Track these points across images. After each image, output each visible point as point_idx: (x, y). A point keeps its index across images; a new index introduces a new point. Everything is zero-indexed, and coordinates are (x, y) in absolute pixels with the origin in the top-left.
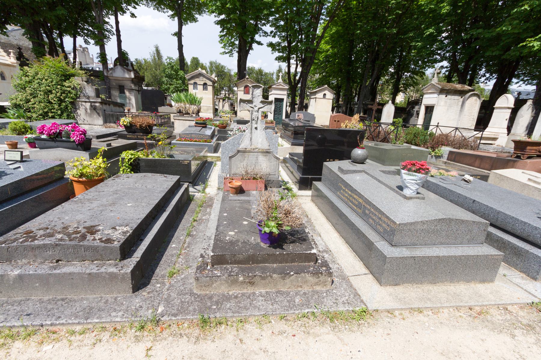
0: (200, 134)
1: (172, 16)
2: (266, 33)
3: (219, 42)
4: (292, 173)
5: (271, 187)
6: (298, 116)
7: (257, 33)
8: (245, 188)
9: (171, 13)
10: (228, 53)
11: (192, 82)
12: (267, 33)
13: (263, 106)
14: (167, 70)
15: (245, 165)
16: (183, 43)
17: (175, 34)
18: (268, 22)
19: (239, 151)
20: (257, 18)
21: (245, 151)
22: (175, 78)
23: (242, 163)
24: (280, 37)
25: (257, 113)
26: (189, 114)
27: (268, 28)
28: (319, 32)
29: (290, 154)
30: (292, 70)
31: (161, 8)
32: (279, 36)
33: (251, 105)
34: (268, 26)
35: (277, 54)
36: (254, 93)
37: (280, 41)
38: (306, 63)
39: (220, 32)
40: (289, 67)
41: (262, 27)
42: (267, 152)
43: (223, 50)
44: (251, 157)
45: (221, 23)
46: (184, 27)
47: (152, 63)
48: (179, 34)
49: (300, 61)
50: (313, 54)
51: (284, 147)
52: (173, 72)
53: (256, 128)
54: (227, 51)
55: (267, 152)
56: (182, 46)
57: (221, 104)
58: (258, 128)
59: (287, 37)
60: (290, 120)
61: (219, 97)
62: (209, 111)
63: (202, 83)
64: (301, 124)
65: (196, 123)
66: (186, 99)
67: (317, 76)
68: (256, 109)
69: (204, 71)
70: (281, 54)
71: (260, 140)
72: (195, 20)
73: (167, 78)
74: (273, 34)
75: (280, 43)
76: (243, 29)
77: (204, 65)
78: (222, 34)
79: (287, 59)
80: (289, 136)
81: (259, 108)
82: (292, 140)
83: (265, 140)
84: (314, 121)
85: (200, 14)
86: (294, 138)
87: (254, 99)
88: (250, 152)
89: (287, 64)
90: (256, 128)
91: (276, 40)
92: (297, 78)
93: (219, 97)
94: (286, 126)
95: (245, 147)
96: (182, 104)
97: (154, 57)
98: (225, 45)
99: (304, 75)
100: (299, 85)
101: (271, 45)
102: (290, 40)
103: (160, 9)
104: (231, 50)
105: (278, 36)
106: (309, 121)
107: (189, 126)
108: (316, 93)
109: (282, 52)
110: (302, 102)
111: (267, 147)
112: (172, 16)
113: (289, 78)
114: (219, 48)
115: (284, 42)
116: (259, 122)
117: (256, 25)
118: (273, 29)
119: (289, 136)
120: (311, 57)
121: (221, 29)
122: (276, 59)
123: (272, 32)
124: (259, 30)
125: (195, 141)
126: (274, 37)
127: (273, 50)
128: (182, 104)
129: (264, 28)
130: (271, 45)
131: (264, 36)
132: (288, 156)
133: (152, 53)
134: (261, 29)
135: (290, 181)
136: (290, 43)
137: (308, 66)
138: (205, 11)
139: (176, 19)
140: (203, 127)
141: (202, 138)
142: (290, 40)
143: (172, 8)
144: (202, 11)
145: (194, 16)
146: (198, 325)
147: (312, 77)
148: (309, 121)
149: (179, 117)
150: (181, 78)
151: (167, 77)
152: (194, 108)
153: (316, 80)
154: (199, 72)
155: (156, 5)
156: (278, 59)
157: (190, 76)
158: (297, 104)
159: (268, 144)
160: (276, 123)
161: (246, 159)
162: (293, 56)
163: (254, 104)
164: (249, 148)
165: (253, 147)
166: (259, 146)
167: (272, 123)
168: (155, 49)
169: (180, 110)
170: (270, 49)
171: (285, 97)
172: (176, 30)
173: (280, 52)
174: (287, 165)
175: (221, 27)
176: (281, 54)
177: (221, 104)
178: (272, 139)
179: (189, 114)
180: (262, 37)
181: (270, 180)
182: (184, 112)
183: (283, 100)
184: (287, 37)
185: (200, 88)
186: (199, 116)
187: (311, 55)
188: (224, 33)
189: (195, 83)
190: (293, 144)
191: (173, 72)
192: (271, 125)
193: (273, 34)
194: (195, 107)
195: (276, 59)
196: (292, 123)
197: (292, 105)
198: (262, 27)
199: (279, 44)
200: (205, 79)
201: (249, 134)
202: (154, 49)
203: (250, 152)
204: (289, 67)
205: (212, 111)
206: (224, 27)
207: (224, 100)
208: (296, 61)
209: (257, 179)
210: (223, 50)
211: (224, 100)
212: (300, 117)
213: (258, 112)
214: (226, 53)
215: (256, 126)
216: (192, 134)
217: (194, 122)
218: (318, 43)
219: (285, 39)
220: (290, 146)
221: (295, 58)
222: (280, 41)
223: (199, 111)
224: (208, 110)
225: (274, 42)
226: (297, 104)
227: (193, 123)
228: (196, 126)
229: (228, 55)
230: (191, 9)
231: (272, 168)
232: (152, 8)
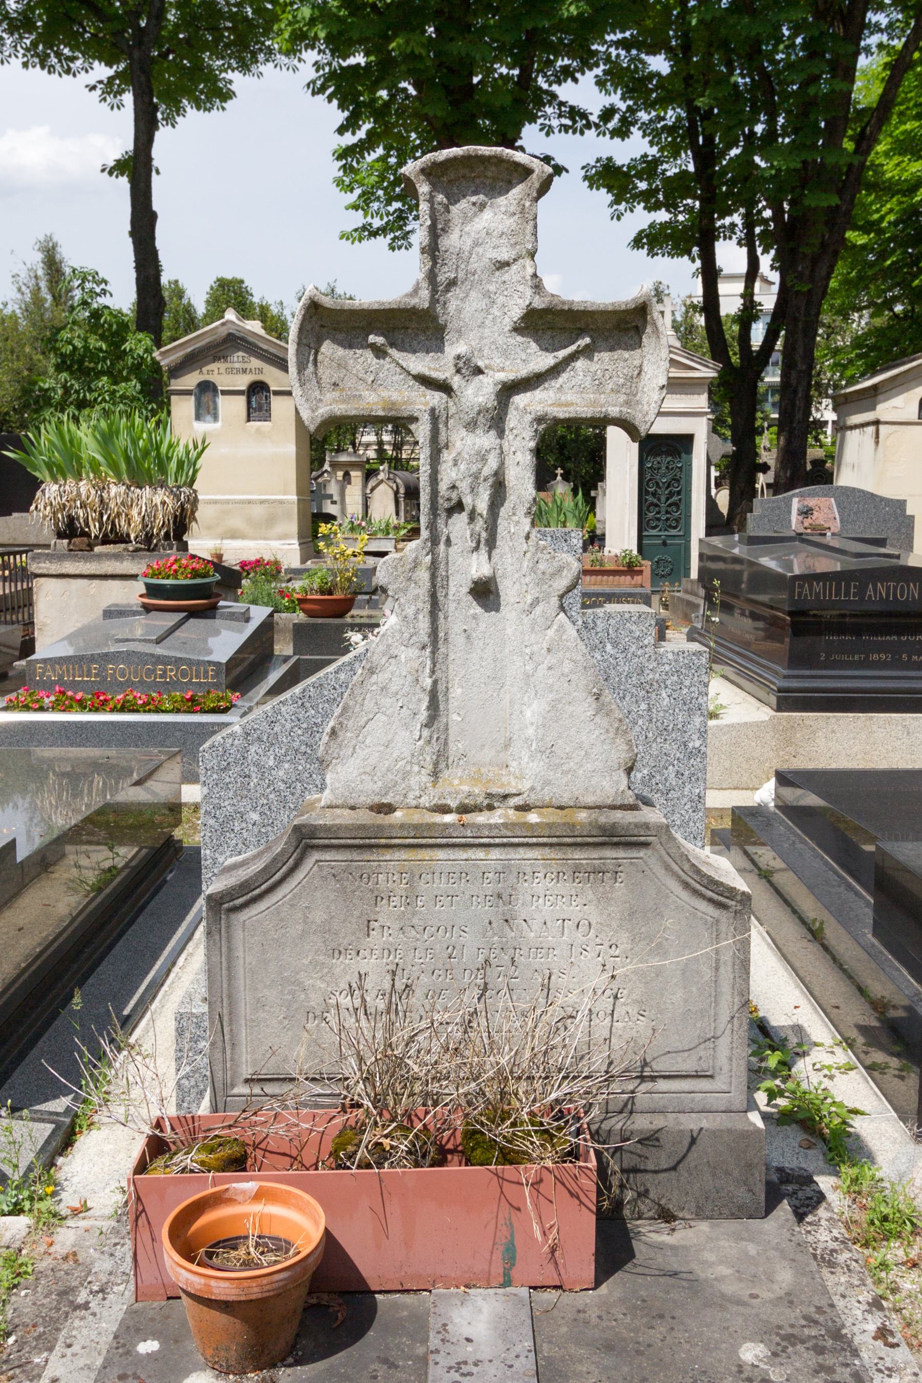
0: (160, 660)
1: (110, 88)
2: (575, 113)
3: (339, 182)
4: (815, 934)
5: (666, 1216)
6: (806, 512)
7: (533, 119)
8: (370, 1261)
9: (102, 71)
10: (382, 231)
11: (190, 380)
12: (584, 115)
13: (544, 361)
14: (65, 335)
15: (377, 981)
16: (158, 204)
17: (120, 167)
18: (587, 60)
19: (306, 840)
20: (530, 49)
21: (370, 837)
22: (108, 373)
23: (346, 968)
24: (652, 132)
25: (486, 440)
26: (123, 539)
27: (585, 92)
28: (866, 89)
29: (783, 779)
30: (730, 302)
31: (58, 55)
32: (646, 129)
33: (419, 363)
34: (588, 79)
35: (641, 218)
36: (451, 241)
37: (654, 151)
38: (804, 248)
39: (341, 130)
40: (710, 275)
41: (555, 88)
42: (613, 838)
43: (357, 219)
44: (447, 898)
45: (343, 87)
46: (163, 137)
47: (23, 322)
48: (137, 168)
49: (768, 240)
50: (840, 193)
51: (727, 718)
52: (95, 342)
53: (485, 592)
54: (377, 223)
55: (613, 838)
56: (153, 216)
57: (354, 493)
58: (508, 591)
59: (692, 133)
60: (753, 541)
61: (343, 458)
62: (280, 529)
63: (242, 382)
64: (826, 564)
65: (153, 591)
66: (107, 455)
67: (860, 322)
68: (478, 393)
69: (254, 326)
70: (662, 216)
71: (533, 711)
72: (221, 94)
73: (64, 375)
74: (613, 123)
75: (656, 162)
76: (455, 104)
77: (274, 310)
78: (349, 139)
79: (697, 239)
80: (746, 645)
81: (509, 390)
82: (779, 676)
83: (584, 707)
84: (908, 544)
85: (245, 67)
86: (797, 660)
87: (453, 301)
88: (422, 839)
89: (698, 263)
90: (485, 592)
91: (634, 148)
92: (758, 333)
93: (343, 458)
94: (726, 587)
95: (370, 790)
96: (84, 487)
97: (37, 291)
98: (367, 198)
99: (797, 313)
100: (772, 377)
101: (608, 176)
102: (709, 140)
103: (54, 60)
104: (401, 217)
105: (644, 128)
106: (881, 542)
107: (109, 614)
108: (873, 396)
109: (670, 205)
110: (792, 455)
111: (610, 786)
112: (110, 88)
113: (712, 332)
114: (339, 210)
115: (676, 155)
116: (515, 522)
117: (526, 80)
118: (615, 99)
119: (746, 645)
120: (833, 211)
121: (340, 117)
122: (637, 243)
123: (608, 113)
124: (540, 104)
125: (123, 709)
126: (622, 133)
127: (617, 202)
128: (84, 487)
129: (566, 92)
130: (608, 176)
131: (565, 128)
132: (765, 794)
133: (24, 275)
134: (554, 96)
135: (819, 1030)
136: (706, 157)
137: (815, 261)
138: (270, 52)
139: (128, 98)
140: (193, 613)
141: (174, 685)
142: (709, 140)
143: (102, 50)
144: (254, 55)
145: (216, 79)
146: (547, 783)
147: (832, 331)
148: (881, 542)
149: (61, 558)
150: (136, 369)
151: (69, 369)
152: (153, 501)
153: (858, 342)
154: (223, 332)
155: (34, 44)
156: (651, 240)
157: (181, 354)
158: (765, 468)
159: (619, 753)
160: (656, 576)
161: (386, 914)
162: (727, 221)
163: (455, 348)
164: (415, 795)
165: (458, 785)
166: (525, 774)
167: (631, 569)
168: (39, 256)
169: (71, 520)
170: (604, 196)
171: (700, 429)
172: (122, 142)
173: (652, 207)
174: (767, 856)
175: (342, 107)
176: (662, 216)
177: (354, 493)
178: (649, 689)
179: (123, 539)
180: (558, 138)
181: (651, 1139)
182: (94, 530)
183: (684, 442)
184: (692, 133)
185: (232, 408)
186: (184, 547)
187: (835, 200)
188: (361, 134)
189: (207, 389)
190: (788, 701)
191: (95, 342)
192: (625, 583)
193: (613, 123)
194: (160, 496)
195: (637, 243)
196: (768, 562)
197: (739, 471)
198: (555, 88)
199: (649, 168)
200: (255, 363)
201: (411, 657)
202: (37, 258)
203: (422, 839)
204: (710, 275)
205: (293, 527)
206: (358, 105)
207: (369, 474)
208: (749, 242)
209: (510, 1157)
210: (357, 219)
211: (369, 474)
212: (818, 518)
213: (496, 421)
214: (374, 234)
215: (478, 567)
216: (107, 658)
217: (139, 587)
218: (865, 142)
219: (674, 139)
220: (764, 714)
221: (739, 234)
222: (654, 151)
223: (180, 525)
224: (271, 521)
225: (622, 160)
226: (765, 468)
227: (131, 594)
228: (147, 609)
229: (383, 242)
230: (206, 46)
231: (676, 997)
232: (16, 63)
